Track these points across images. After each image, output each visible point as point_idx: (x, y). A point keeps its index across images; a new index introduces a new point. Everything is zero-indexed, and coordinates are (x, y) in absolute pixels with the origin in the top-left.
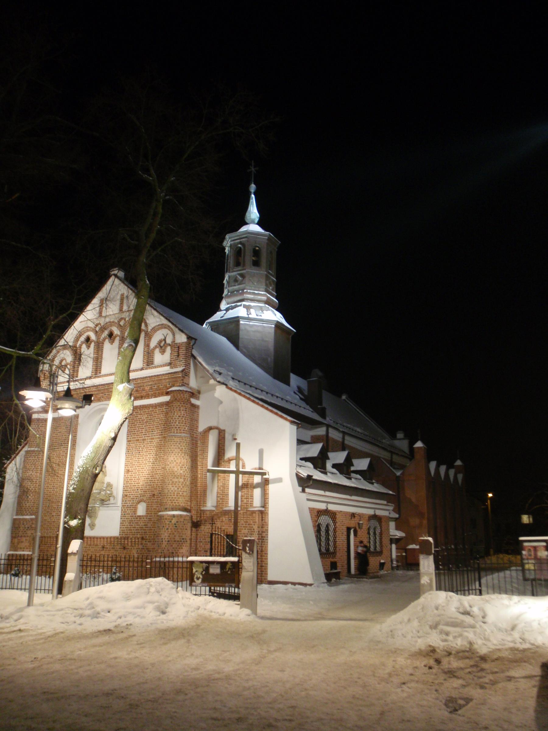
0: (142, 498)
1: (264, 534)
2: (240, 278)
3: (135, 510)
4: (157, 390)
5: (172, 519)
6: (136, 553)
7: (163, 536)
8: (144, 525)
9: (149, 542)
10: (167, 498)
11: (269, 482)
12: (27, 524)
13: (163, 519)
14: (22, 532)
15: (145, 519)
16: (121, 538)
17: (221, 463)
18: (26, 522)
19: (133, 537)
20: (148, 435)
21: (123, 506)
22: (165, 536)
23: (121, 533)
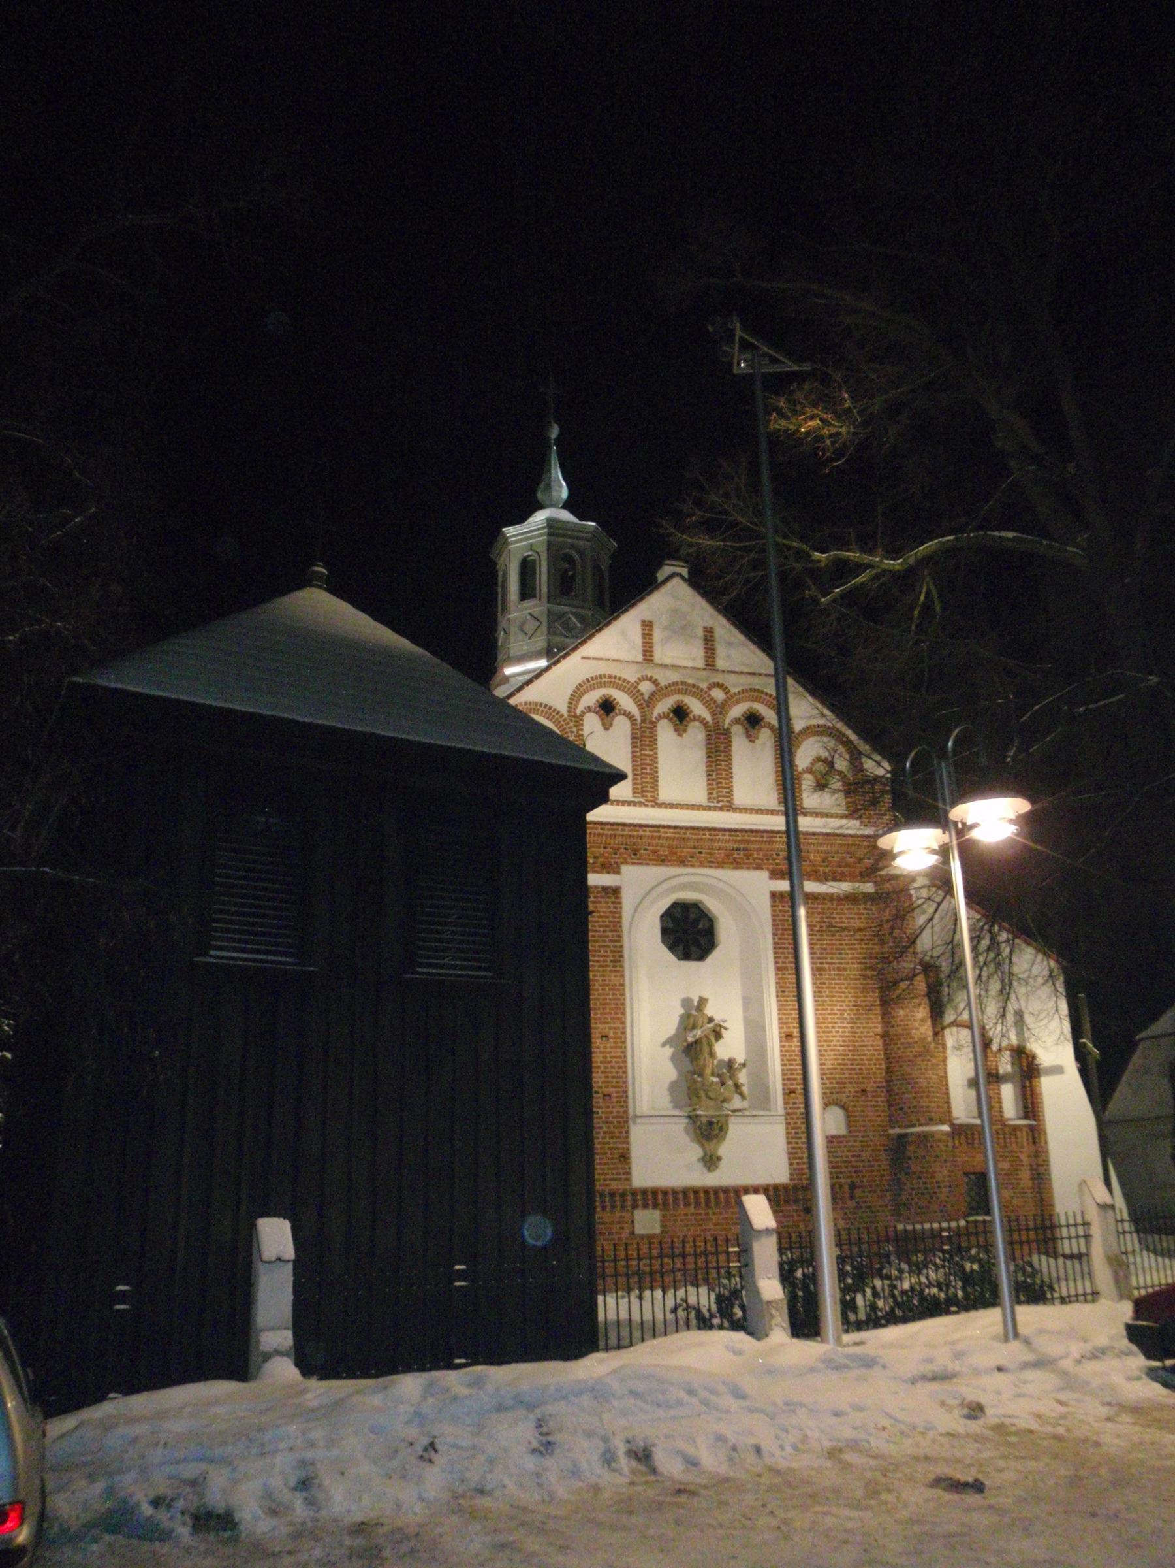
0: (835, 1096)
1: (1041, 1169)
2: (579, 625)
4: (840, 866)
6: (843, 1219)
7: (939, 1177)
8: (853, 1156)
9: (870, 1192)
10: (927, 1097)
11: (1039, 1073)
16: (795, 1188)
20: (829, 960)
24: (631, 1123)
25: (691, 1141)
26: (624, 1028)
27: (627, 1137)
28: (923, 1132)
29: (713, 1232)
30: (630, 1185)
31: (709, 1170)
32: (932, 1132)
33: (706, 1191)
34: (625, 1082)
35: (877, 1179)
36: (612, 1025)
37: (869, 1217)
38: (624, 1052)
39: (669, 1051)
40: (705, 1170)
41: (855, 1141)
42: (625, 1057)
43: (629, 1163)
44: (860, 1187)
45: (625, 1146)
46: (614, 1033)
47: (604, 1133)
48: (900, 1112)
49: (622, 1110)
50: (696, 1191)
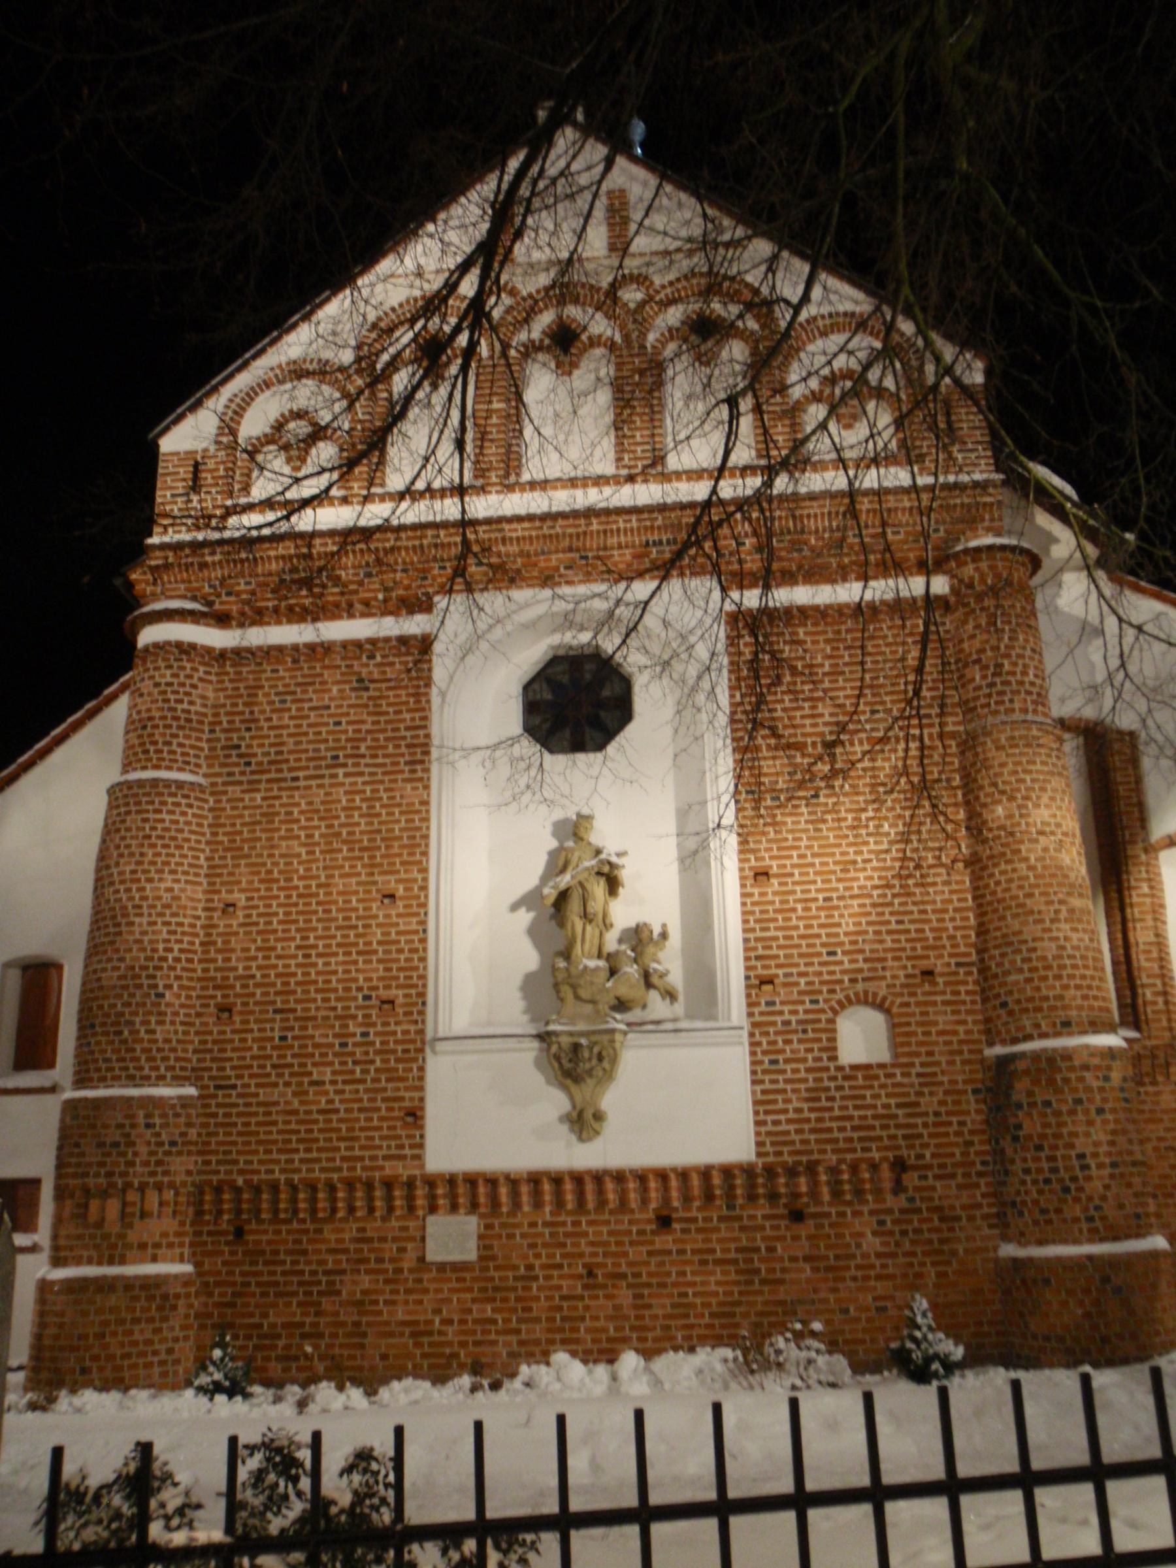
0: (860, 986)
3: (830, 1040)
5: (1109, 1068)
6: (874, 1233)
7: (1082, 1145)
10: (1058, 977)
12: (165, 1126)
13: (1072, 1069)
14: (146, 1164)
15: (899, 1079)
16: (769, 1171)
17: (1137, 857)
18: (164, 1116)
19: (840, 1161)
21: (755, 1025)
22: (1096, 1144)
23: (769, 1148)
24: (428, 1050)
25: (548, 1082)
26: (425, 880)
27: (421, 1078)
28: (1044, 1050)
29: (587, 1260)
30: (423, 1166)
31: (581, 1139)
32: (1065, 1049)
33: (578, 1178)
34: (423, 977)
35: (957, 1152)
36: (403, 876)
37: (937, 1230)
38: (423, 923)
39: (525, 917)
40: (573, 1138)
41: (908, 1075)
42: (425, 931)
43: (422, 1127)
44: (915, 1168)
45: (416, 1094)
46: (406, 889)
47: (377, 1070)
48: (1002, 1012)
49: (412, 1028)
50: (557, 1179)
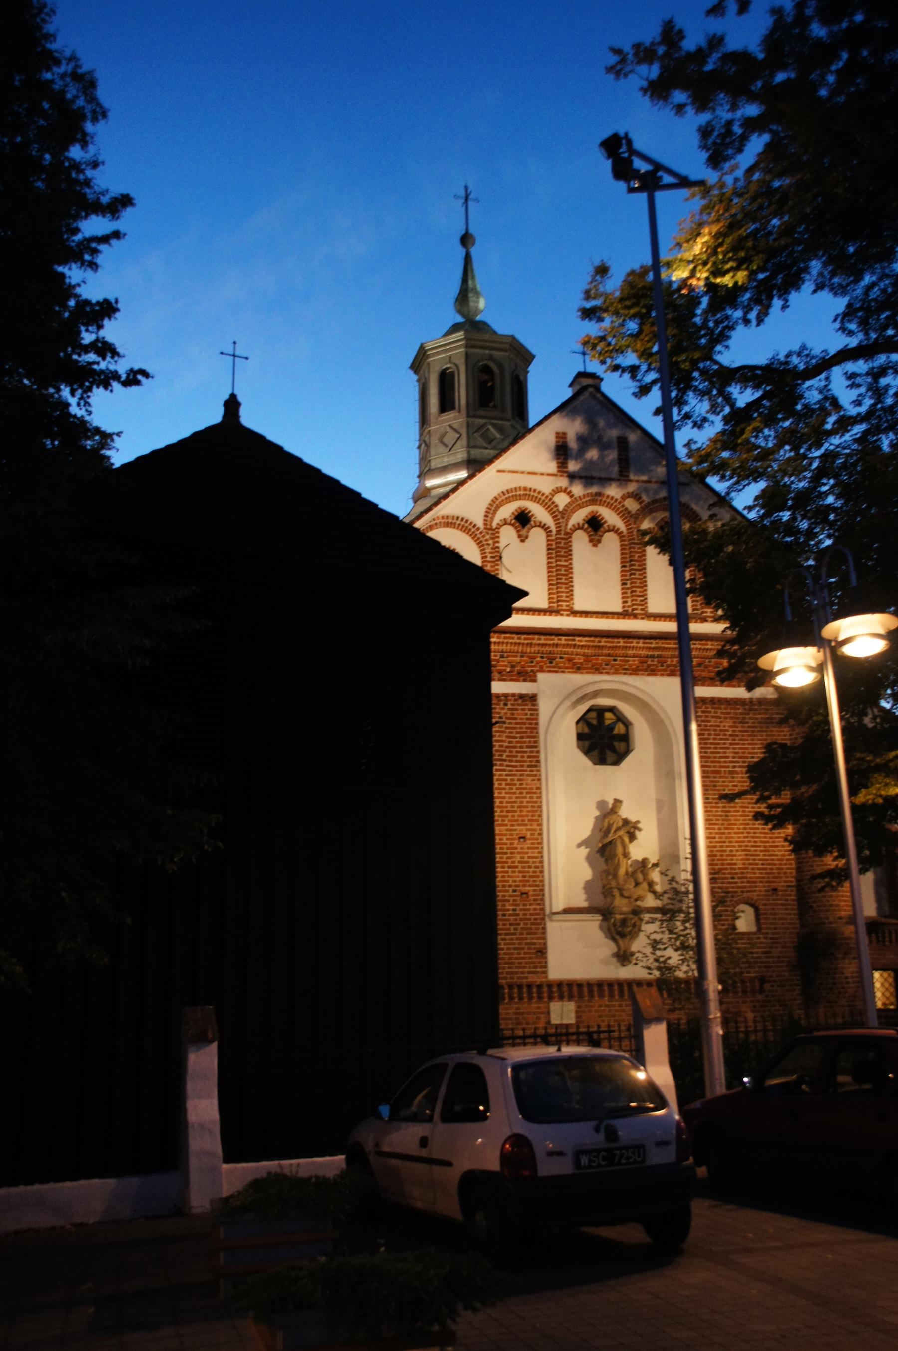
6: (753, 1012)
15: (762, 940)
